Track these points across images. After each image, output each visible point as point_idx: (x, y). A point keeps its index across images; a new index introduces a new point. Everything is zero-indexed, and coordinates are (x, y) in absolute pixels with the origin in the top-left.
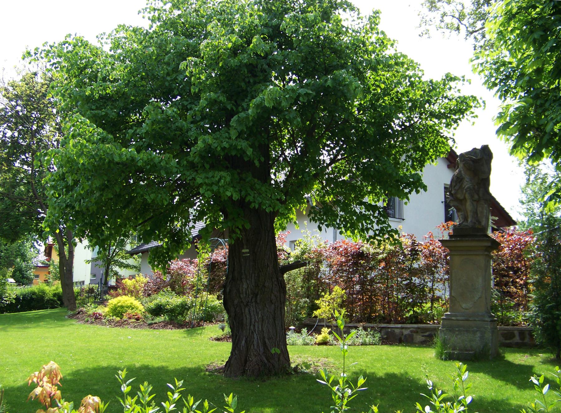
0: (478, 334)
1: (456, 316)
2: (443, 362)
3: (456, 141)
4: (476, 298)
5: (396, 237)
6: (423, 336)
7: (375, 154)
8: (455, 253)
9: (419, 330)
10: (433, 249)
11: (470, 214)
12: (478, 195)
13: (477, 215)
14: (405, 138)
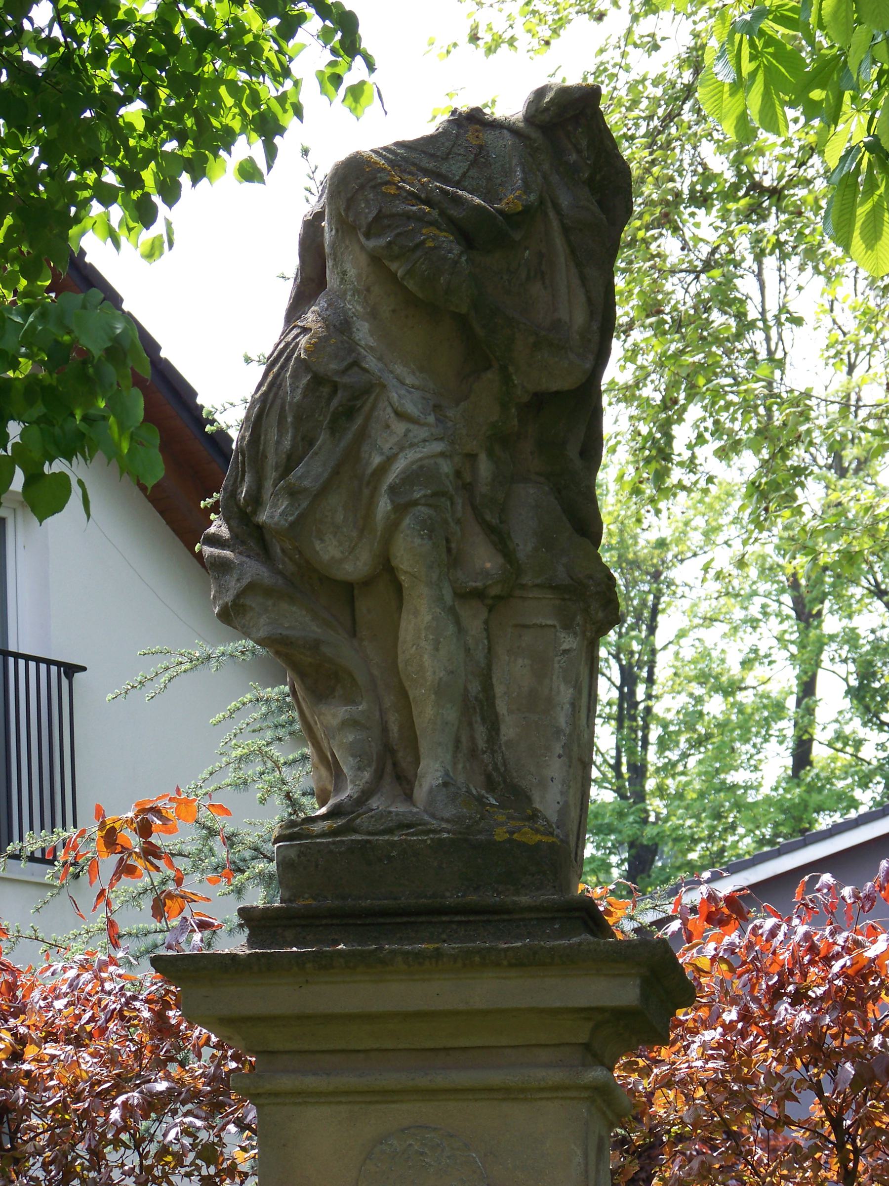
3: (368, 38)
8: (311, 1082)
13: (494, 727)
14: (849, 1147)
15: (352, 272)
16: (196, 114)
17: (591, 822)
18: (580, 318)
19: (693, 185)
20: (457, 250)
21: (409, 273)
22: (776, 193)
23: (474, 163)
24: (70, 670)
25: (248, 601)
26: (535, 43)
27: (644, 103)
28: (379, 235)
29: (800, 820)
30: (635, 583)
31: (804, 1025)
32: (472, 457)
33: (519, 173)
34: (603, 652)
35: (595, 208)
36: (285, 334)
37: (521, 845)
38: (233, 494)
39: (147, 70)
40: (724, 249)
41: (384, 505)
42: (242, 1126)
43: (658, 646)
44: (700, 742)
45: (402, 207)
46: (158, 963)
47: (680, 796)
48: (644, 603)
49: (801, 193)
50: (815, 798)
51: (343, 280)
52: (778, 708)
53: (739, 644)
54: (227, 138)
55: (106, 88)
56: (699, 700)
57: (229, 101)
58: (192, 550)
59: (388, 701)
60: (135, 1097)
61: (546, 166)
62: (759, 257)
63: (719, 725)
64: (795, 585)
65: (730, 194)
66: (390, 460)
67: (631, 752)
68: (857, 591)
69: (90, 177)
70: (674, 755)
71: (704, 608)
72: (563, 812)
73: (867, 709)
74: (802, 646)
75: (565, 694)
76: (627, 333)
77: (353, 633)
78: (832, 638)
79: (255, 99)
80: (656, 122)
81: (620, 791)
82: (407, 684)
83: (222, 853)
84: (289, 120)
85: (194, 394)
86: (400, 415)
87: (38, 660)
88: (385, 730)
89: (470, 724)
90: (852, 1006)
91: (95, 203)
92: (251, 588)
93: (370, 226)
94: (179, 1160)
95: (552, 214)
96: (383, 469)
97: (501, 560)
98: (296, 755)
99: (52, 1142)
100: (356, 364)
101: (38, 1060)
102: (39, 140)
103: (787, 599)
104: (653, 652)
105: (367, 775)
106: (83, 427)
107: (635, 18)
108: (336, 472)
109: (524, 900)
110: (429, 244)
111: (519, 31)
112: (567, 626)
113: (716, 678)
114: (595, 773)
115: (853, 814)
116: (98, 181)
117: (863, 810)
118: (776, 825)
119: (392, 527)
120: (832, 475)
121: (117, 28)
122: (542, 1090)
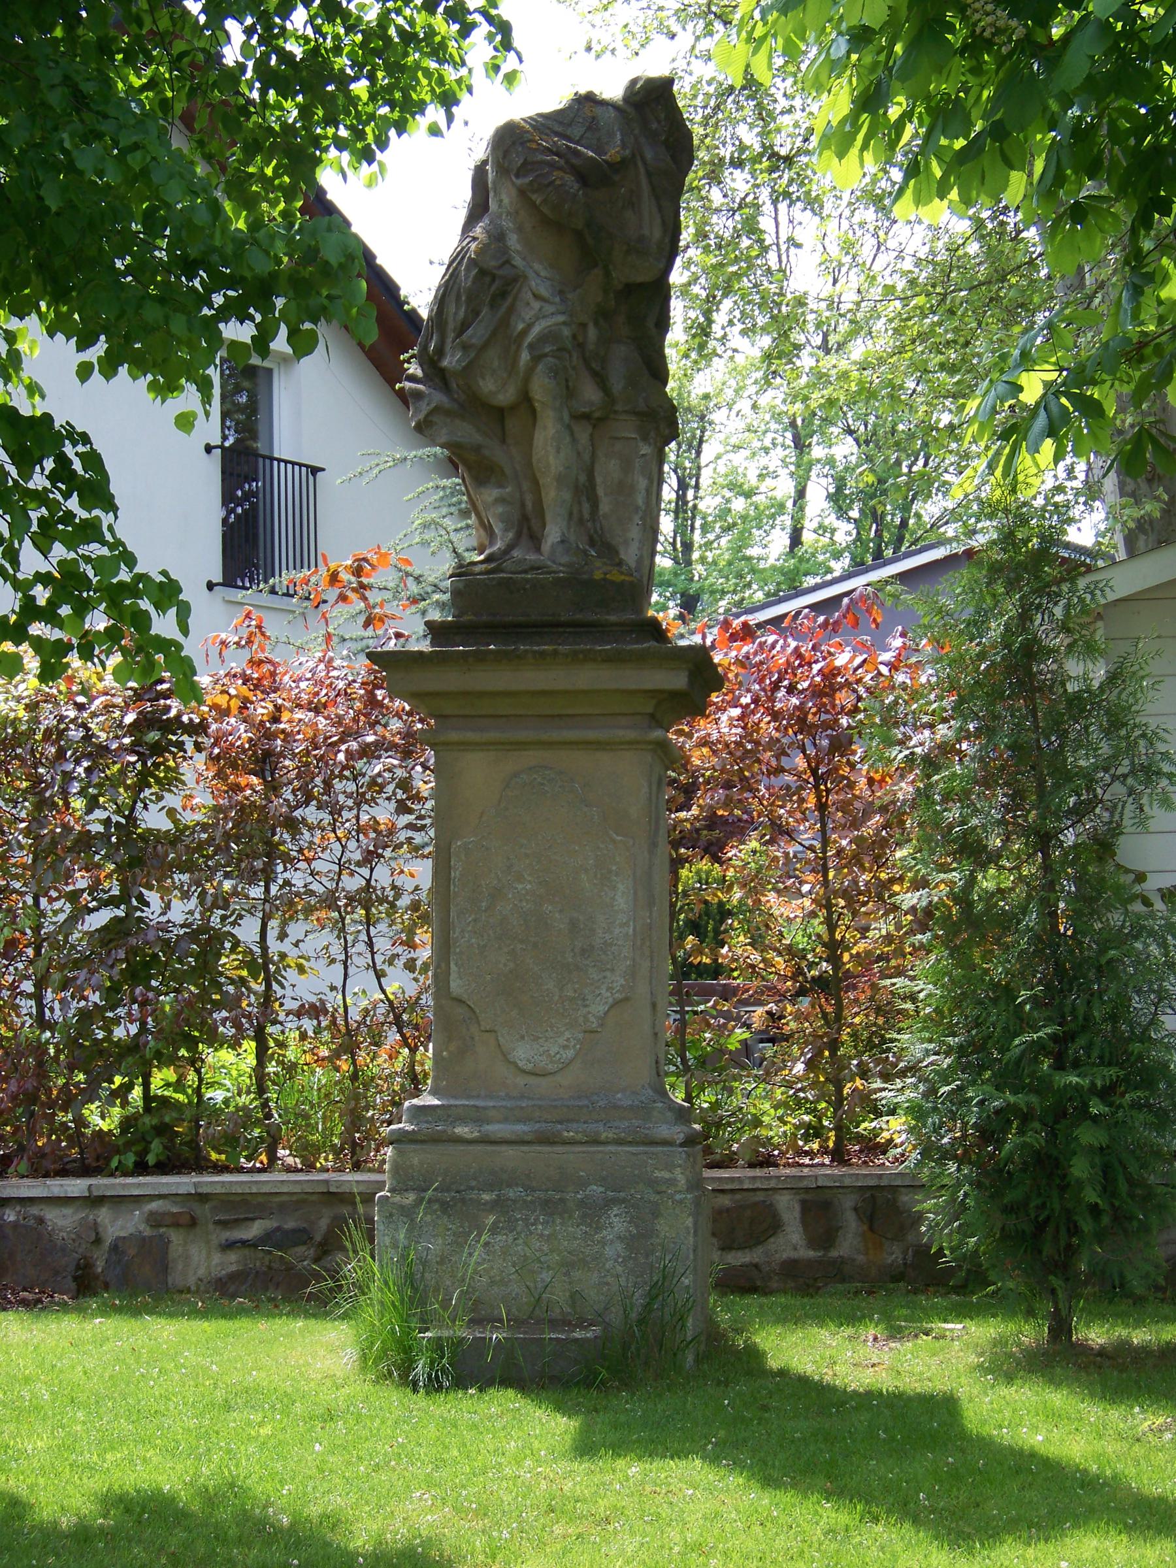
0: (617, 1223)
1: (477, 1117)
2: (420, 1400)
3: (517, 40)
4: (599, 1008)
5: (164, 625)
6: (229, 1246)
7: (67, 80)
8: (470, 736)
9: (203, 1211)
10: (276, 720)
11: (554, 497)
12: (601, 380)
13: (595, 503)
15: (506, 201)
16: (402, 90)
17: (657, 580)
18: (657, 234)
19: (732, 153)
20: (576, 186)
21: (545, 201)
22: (789, 160)
23: (589, 128)
24: (315, 470)
25: (435, 419)
26: (629, 53)
27: (701, 97)
28: (525, 176)
29: (794, 580)
30: (689, 422)
31: (796, 707)
32: (583, 326)
33: (619, 136)
34: (666, 468)
35: (669, 159)
36: (461, 241)
37: (612, 582)
38: (424, 348)
39: (369, 58)
40: (751, 197)
41: (525, 356)
42: (425, 767)
43: (703, 464)
44: (727, 529)
45: (540, 157)
46: (372, 656)
47: (715, 563)
48: (694, 436)
49: (804, 159)
50: (804, 566)
51: (500, 206)
52: (782, 506)
53: (756, 464)
54: (421, 107)
55: (342, 71)
56: (728, 501)
57: (424, 82)
58: (393, 388)
59: (526, 486)
60: (354, 745)
61: (636, 132)
62: (775, 202)
63: (740, 518)
64: (793, 424)
65: (756, 159)
66: (529, 326)
67: (683, 535)
68: (835, 430)
69: (330, 131)
70: (711, 536)
71: (734, 440)
72: (640, 561)
73: (840, 508)
74: (798, 466)
75: (642, 483)
76: (685, 251)
77: (503, 441)
78: (818, 461)
79: (441, 81)
80: (709, 110)
81: (675, 560)
82: (538, 475)
83: (414, 588)
84: (464, 96)
85: (398, 289)
86: (537, 297)
87: (293, 464)
88: (523, 505)
89: (580, 503)
90: (826, 695)
91: (332, 149)
92: (437, 410)
93: (519, 169)
94: (382, 787)
95: (640, 164)
96: (525, 332)
97: (601, 394)
98: (463, 524)
99: (298, 777)
100: (508, 262)
101: (290, 721)
102: (297, 106)
103: (789, 435)
104: (699, 468)
105: (511, 535)
106: (326, 302)
107: (698, 38)
108: (494, 334)
109: (613, 618)
110: (558, 182)
111: (619, 45)
112: (645, 438)
113: (741, 486)
114: (659, 548)
115: (829, 577)
116: (335, 136)
117: (837, 574)
118: (778, 584)
119: (530, 371)
120: (821, 353)
121: (349, 29)
122: (622, 743)
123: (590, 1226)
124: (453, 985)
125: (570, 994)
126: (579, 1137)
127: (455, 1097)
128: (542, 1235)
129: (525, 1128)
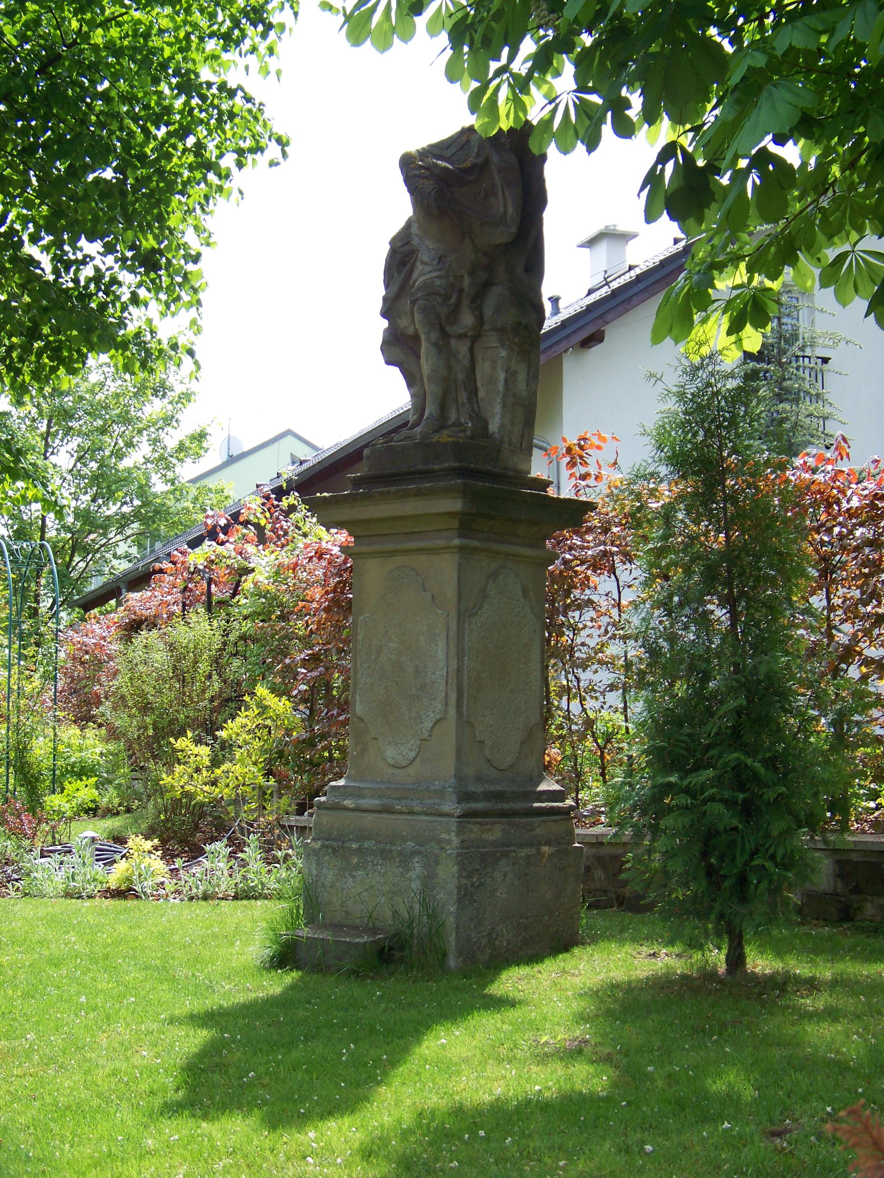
0: (417, 867)
13: (476, 392)
109: (437, 467)
112: (503, 346)
123: (403, 868)
124: (357, 708)
125: (414, 715)
126: (404, 809)
127: (355, 781)
128: (380, 873)
129: (378, 802)
